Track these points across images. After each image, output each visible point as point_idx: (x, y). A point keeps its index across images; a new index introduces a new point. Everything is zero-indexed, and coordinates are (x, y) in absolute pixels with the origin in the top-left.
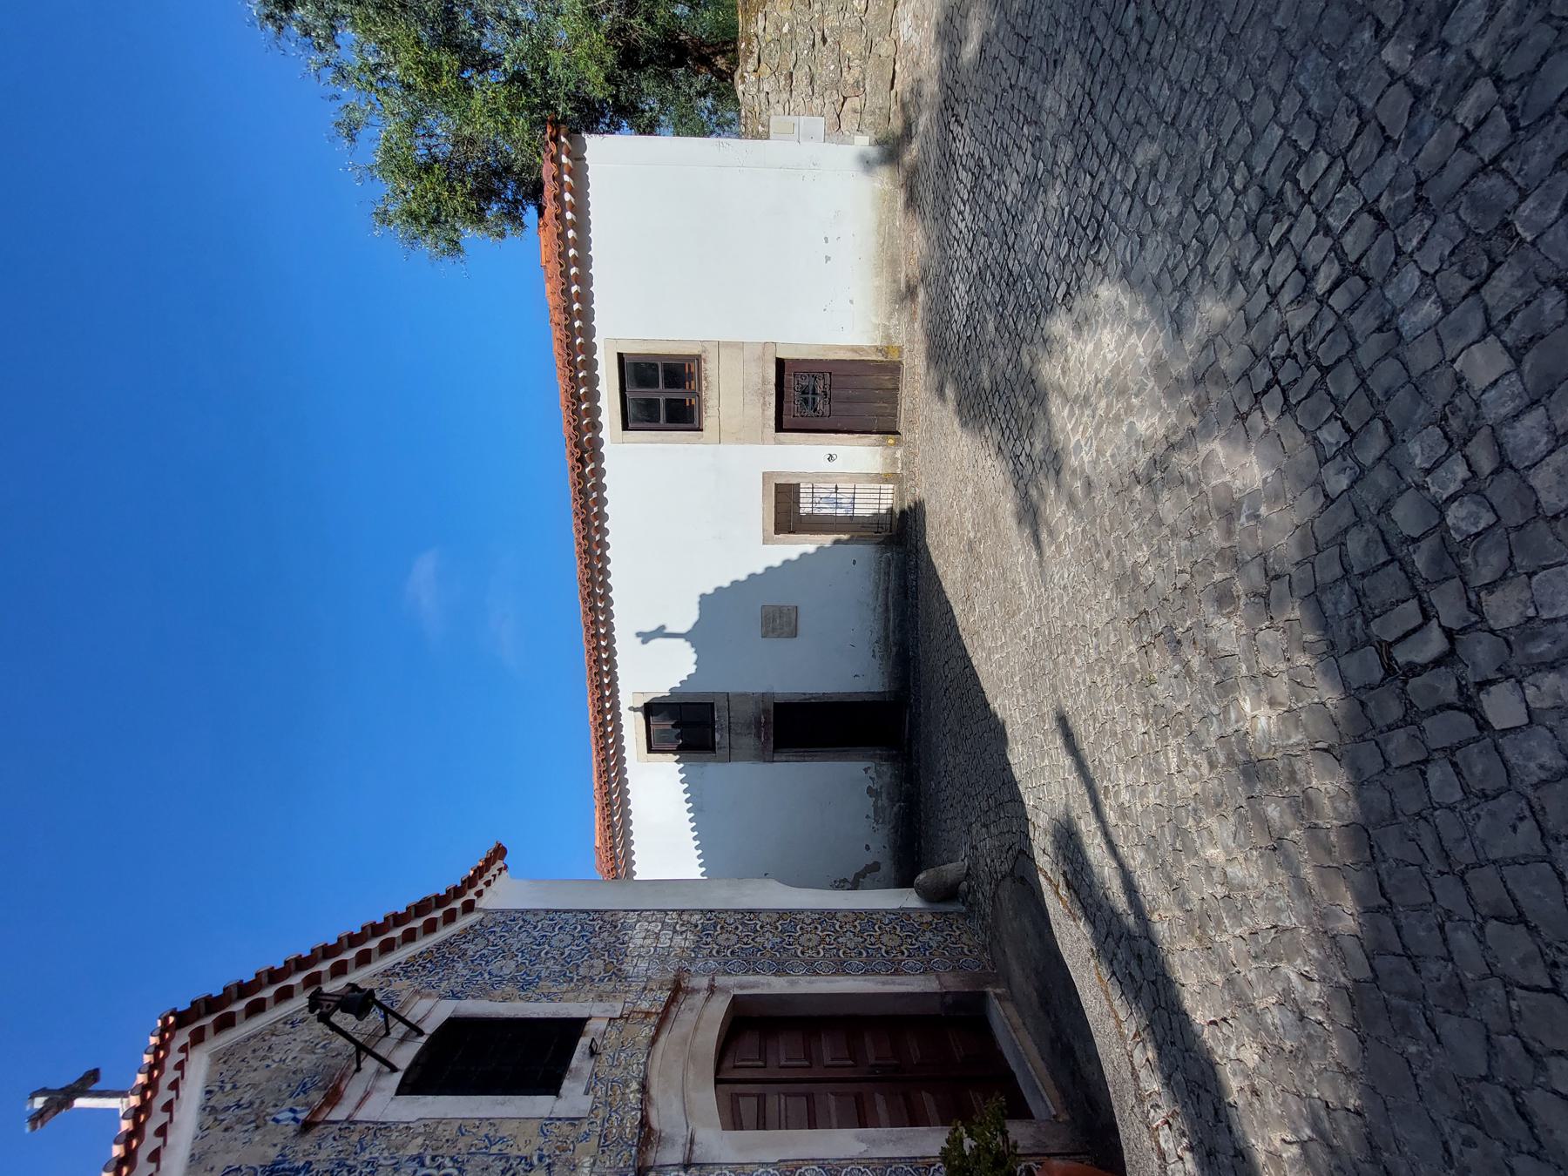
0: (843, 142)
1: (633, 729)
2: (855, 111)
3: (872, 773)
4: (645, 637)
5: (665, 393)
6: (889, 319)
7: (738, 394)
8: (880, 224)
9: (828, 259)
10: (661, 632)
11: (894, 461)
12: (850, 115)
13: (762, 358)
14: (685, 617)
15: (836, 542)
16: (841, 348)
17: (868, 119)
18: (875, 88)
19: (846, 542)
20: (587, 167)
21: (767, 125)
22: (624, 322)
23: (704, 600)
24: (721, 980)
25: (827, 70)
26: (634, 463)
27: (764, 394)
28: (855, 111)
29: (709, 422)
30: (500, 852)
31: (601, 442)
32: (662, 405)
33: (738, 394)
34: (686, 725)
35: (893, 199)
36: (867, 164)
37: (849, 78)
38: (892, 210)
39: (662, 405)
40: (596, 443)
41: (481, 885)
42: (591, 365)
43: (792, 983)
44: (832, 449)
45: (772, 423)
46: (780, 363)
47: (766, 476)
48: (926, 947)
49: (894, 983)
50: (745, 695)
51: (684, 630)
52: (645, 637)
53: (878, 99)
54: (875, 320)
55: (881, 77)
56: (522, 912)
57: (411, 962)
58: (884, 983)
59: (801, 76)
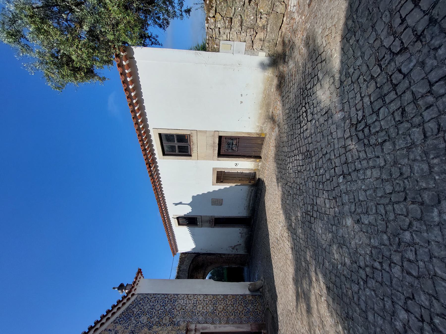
0: (253, 54)
1: (174, 222)
2: (261, 40)
4: (176, 204)
5: (178, 145)
6: (263, 124)
7: (204, 146)
8: (265, 90)
9: (241, 102)
10: (180, 203)
11: (258, 166)
12: (258, 42)
13: (213, 136)
14: (190, 200)
15: (236, 185)
16: (243, 133)
17: (266, 44)
18: (272, 29)
19: (239, 185)
20: (136, 62)
21: (218, 45)
22: (160, 121)
23: (193, 197)
24: (199, 326)
25: (249, 19)
26: (167, 166)
27: (214, 147)
28: (261, 40)
29: (194, 154)
30: (140, 271)
31: (156, 159)
32: (177, 148)
33: (204, 146)
34: (189, 221)
35: (272, 81)
36: (263, 66)
37: (260, 23)
38: (271, 85)
39: (177, 148)
40: (154, 160)
41: (135, 287)
42: (148, 137)
43: (215, 327)
44: (237, 162)
45: (217, 155)
46: (220, 137)
47: (214, 169)
48: (249, 311)
49: (240, 328)
51: (188, 203)
52: (176, 204)
53: (273, 35)
54: (257, 124)
55: (276, 24)
56: (147, 294)
57: (120, 317)
58: (238, 327)
59: (236, 21)
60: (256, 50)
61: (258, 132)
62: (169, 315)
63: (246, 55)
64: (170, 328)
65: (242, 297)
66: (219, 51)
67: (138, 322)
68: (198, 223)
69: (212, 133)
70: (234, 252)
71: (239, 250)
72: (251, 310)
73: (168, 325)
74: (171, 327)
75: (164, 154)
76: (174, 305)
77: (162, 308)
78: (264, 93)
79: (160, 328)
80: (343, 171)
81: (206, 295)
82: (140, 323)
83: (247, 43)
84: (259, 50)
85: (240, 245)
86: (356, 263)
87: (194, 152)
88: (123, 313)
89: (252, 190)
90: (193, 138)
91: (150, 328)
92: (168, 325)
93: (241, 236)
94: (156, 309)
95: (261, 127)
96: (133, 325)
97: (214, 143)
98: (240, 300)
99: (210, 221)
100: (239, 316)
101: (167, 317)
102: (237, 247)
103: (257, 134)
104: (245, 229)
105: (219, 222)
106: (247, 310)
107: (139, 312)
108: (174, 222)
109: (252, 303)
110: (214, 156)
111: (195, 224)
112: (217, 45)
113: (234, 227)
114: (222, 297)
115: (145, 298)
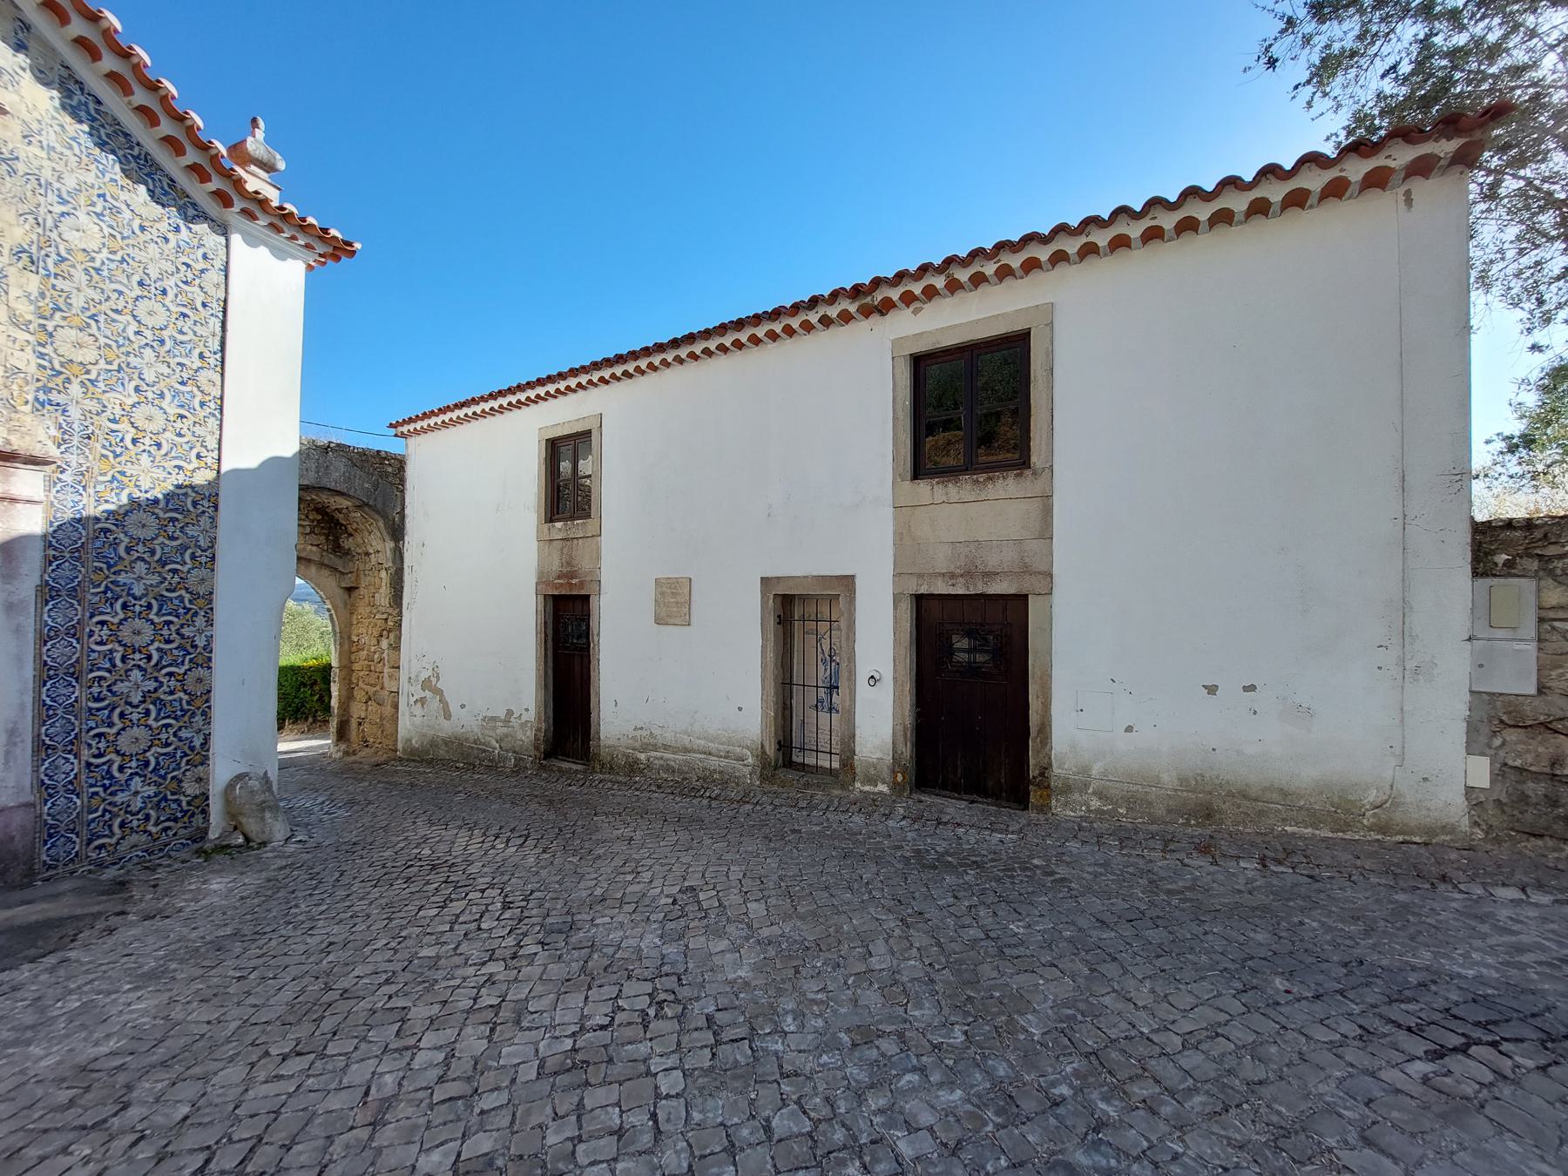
1: (562, 414)
8: (1284, 793)
9: (1212, 690)
13: (1026, 570)
27: (968, 574)
29: (923, 487)
30: (340, 250)
33: (973, 522)
45: (923, 590)
50: (599, 558)
60: (1497, 742)
61: (1056, 770)
62: (102, 364)
63: (1468, 697)
64: (27, 361)
65: (197, 743)
66: (1476, 574)
67: (64, 202)
68: (559, 525)
70: (409, 692)
71: (418, 710)
72: (120, 798)
73: (42, 356)
74: (32, 369)
75: (920, 363)
76: (162, 396)
77: (148, 333)
78: (1265, 789)
79: (25, 310)
81: (213, 558)
82: (58, 209)
83: (1536, 702)
84: (1502, 753)
85: (448, 716)
87: (939, 490)
88: (126, 135)
90: (968, 487)
91: (28, 258)
92: (42, 356)
93: (493, 719)
94: (143, 306)
95: (1087, 786)
96: (46, 174)
97: (989, 575)
98: (183, 734)
99: (572, 575)
100: (86, 737)
101: (89, 355)
102: (434, 704)
103: (1045, 769)
104: (530, 734)
105: (567, 624)
106: (121, 777)
107: (127, 214)
108: (562, 414)
109: (160, 801)
110: (920, 576)
111: (552, 514)
112: (1509, 564)
114: (200, 642)
115: (205, 257)
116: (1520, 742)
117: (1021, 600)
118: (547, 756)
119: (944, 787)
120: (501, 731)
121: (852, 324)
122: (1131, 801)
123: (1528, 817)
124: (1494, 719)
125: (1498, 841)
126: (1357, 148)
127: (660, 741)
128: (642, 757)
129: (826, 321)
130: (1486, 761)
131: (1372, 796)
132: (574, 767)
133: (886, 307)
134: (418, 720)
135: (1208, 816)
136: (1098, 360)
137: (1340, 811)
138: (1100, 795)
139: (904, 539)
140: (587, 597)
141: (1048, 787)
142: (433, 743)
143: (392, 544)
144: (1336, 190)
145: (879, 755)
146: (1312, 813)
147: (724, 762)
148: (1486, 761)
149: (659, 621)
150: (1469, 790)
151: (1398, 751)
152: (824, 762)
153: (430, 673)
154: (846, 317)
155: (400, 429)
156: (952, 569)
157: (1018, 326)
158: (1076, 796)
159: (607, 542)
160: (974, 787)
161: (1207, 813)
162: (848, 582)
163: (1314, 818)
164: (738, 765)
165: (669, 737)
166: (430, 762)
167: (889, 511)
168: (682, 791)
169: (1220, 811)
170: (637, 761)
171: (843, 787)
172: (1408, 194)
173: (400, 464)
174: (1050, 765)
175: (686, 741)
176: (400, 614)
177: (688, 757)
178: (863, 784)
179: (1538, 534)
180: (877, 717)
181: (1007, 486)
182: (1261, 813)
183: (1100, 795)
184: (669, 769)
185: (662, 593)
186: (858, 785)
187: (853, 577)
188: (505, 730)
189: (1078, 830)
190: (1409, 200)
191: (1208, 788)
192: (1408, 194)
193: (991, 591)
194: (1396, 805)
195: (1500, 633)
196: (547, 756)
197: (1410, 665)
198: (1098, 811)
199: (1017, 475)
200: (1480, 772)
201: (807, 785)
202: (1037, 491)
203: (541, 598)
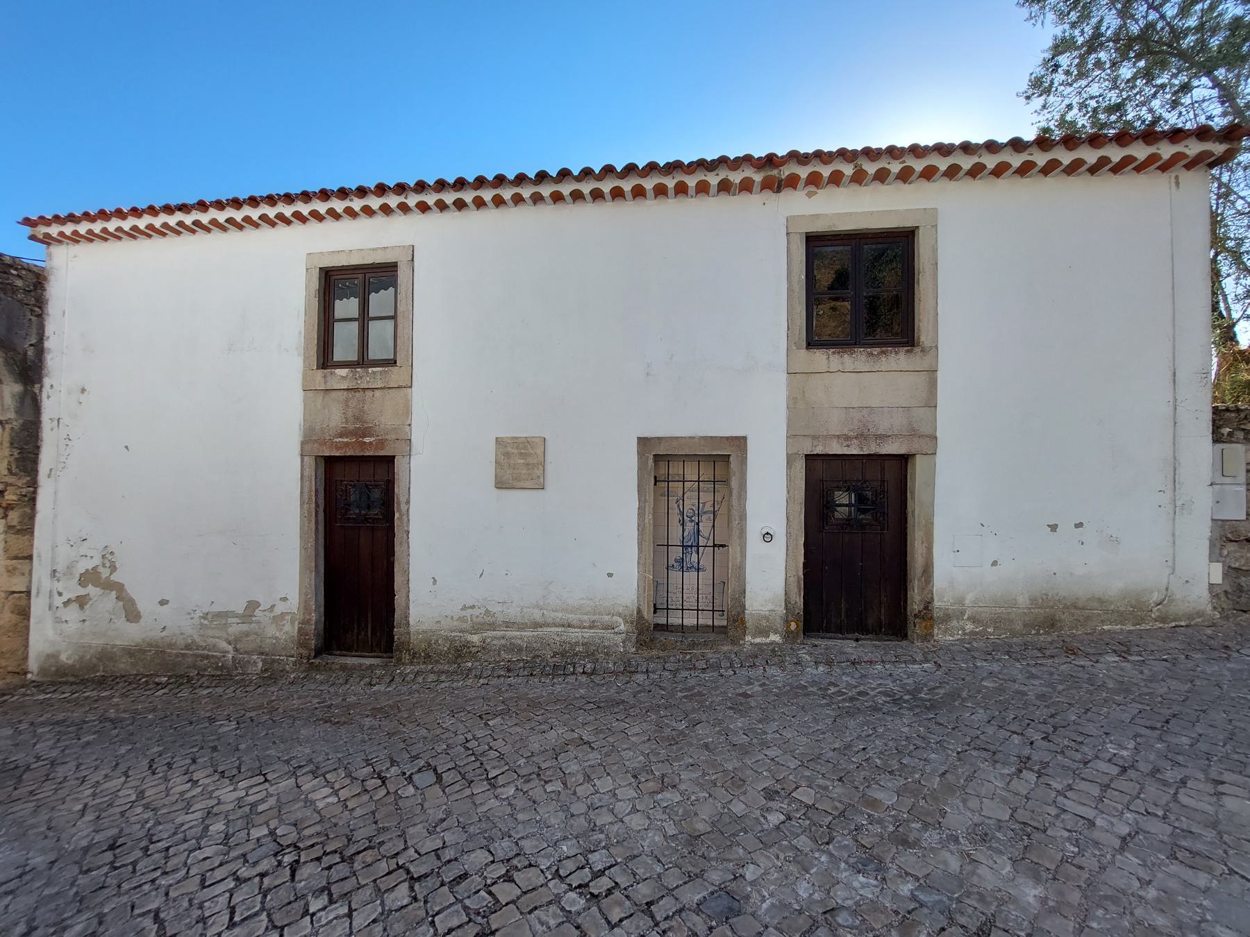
3: (280, 608)
8: (1101, 601)
9: (1054, 528)
13: (913, 434)
21: (1230, 438)
27: (862, 436)
29: (820, 358)
33: (862, 392)
45: (819, 450)
61: (937, 603)
63: (1210, 523)
69: (925, 430)
71: (72, 614)
75: (817, 244)
78: (1089, 599)
80: (356, 505)
85: (133, 615)
86: (100, 923)
89: (610, 627)
90: (863, 358)
95: (963, 613)
97: (882, 438)
99: (366, 432)
103: (928, 605)
110: (814, 437)
112: (1230, 434)
113: (314, 581)
116: (1235, 552)
117: (903, 461)
118: (318, 652)
119: (828, 630)
120: (235, 628)
121: (464, 212)
122: (997, 621)
123: (1243, 600)
124: (1228, 537)
125: (1227, 618)
126: (1043, 142)
127: (500, 618)
128: (475, 639)
129: (725, 187)
130: (1220, 565)
131: (1156, 597)
132: (368, 661)
133: (792, 182)
134: (72, 627)
135: (1053, 625)
136: (969, 260)
137: (1136, 610)
138: (973, 619)
139: (798, 406)
140: (390, 460)
141: (932, 618)
142: (106, 655)
143: (18, 388)
144: (1025, 169)
145: (770, 607)
146: (1121, 614)
147: (588, 634)
148: (1220, 565)
149: (501, 484)
150: (1211, 586)
151: (1170, 563)
152: (690, 620)
153: (97, 561)
154: (746, 186)
155: (42, 230)
156: (846, 431)
157: (908, 224)
158: (954, 623)
159: (421, 398)
160: (857, 627)
161: (1051, 623)
162: (740, 443)
163: (1121, 617)
164: (608, 634)
165: (513, 613)
166: (101, 682)
167: (783, 377)
168: (537, 671)
169: (1060, 621)
170: (467, 645)
171: (733, 643)
172: (1177, 177)
173: (37, 281)
174: (932, 599)
175: (537, 615)
176: (34, 484)
177: (540, 632)
178: (754, 636)
179: (1242, 415)
180: (769, 572)
181: (898, 360)
182: (1088, 618)
183: (973, 619)
184: (513, 648)
185: (507, 455)
186: (748, 638)
187: (745, 438)
188: (245, 627)
189: (967, 649)
190: (1177, 184)
191: (1051, 604)
192: (1177, 177)
193: (367, 454)
194: (1171, 601)
195: (1227, 480)
196: (318, 652)
197: (1179, 503)
198: (973, 633)
199: (908, 351)
200: (1216, 573)
201: (693, 645)
202: (925, 366)
203: (309, 461)
